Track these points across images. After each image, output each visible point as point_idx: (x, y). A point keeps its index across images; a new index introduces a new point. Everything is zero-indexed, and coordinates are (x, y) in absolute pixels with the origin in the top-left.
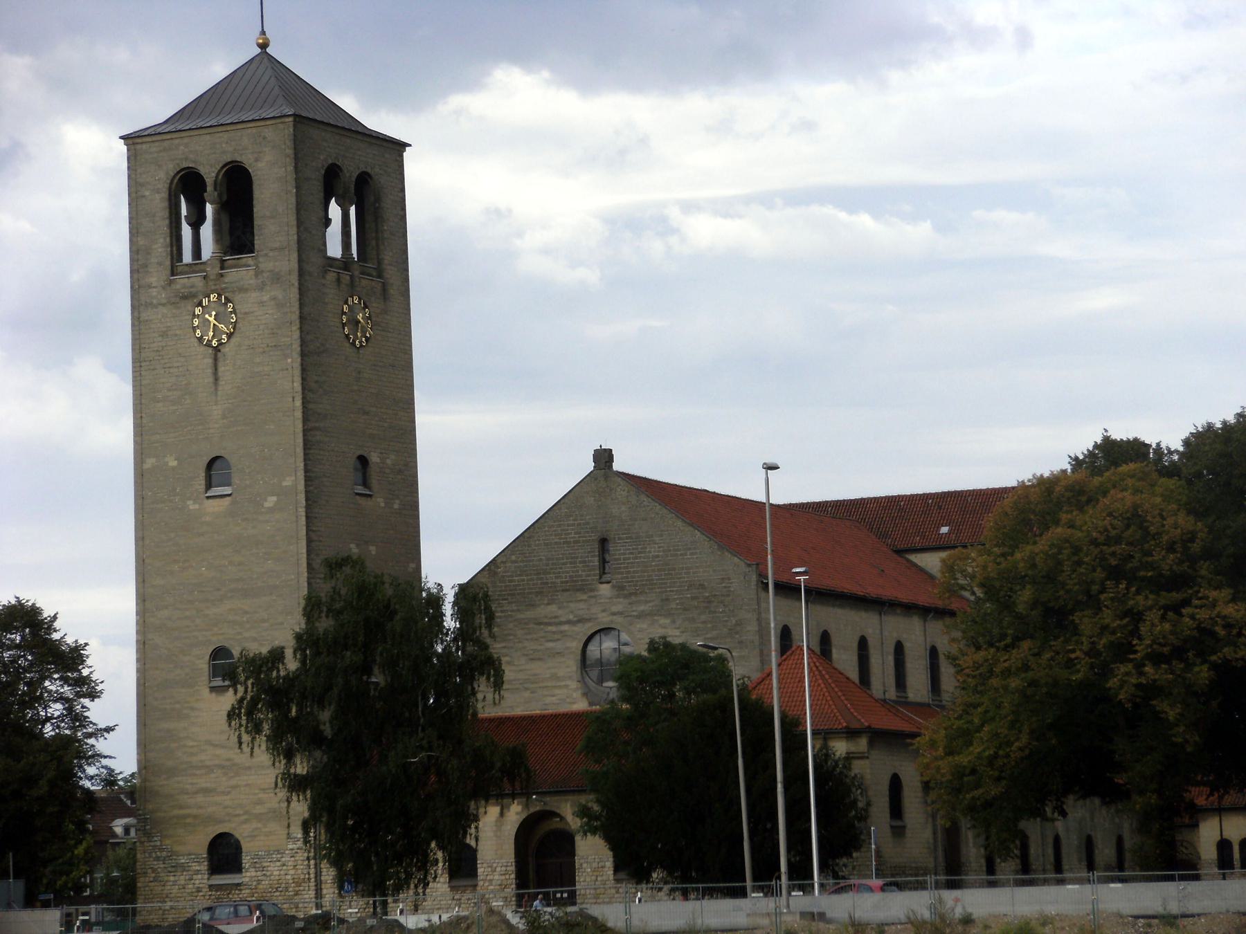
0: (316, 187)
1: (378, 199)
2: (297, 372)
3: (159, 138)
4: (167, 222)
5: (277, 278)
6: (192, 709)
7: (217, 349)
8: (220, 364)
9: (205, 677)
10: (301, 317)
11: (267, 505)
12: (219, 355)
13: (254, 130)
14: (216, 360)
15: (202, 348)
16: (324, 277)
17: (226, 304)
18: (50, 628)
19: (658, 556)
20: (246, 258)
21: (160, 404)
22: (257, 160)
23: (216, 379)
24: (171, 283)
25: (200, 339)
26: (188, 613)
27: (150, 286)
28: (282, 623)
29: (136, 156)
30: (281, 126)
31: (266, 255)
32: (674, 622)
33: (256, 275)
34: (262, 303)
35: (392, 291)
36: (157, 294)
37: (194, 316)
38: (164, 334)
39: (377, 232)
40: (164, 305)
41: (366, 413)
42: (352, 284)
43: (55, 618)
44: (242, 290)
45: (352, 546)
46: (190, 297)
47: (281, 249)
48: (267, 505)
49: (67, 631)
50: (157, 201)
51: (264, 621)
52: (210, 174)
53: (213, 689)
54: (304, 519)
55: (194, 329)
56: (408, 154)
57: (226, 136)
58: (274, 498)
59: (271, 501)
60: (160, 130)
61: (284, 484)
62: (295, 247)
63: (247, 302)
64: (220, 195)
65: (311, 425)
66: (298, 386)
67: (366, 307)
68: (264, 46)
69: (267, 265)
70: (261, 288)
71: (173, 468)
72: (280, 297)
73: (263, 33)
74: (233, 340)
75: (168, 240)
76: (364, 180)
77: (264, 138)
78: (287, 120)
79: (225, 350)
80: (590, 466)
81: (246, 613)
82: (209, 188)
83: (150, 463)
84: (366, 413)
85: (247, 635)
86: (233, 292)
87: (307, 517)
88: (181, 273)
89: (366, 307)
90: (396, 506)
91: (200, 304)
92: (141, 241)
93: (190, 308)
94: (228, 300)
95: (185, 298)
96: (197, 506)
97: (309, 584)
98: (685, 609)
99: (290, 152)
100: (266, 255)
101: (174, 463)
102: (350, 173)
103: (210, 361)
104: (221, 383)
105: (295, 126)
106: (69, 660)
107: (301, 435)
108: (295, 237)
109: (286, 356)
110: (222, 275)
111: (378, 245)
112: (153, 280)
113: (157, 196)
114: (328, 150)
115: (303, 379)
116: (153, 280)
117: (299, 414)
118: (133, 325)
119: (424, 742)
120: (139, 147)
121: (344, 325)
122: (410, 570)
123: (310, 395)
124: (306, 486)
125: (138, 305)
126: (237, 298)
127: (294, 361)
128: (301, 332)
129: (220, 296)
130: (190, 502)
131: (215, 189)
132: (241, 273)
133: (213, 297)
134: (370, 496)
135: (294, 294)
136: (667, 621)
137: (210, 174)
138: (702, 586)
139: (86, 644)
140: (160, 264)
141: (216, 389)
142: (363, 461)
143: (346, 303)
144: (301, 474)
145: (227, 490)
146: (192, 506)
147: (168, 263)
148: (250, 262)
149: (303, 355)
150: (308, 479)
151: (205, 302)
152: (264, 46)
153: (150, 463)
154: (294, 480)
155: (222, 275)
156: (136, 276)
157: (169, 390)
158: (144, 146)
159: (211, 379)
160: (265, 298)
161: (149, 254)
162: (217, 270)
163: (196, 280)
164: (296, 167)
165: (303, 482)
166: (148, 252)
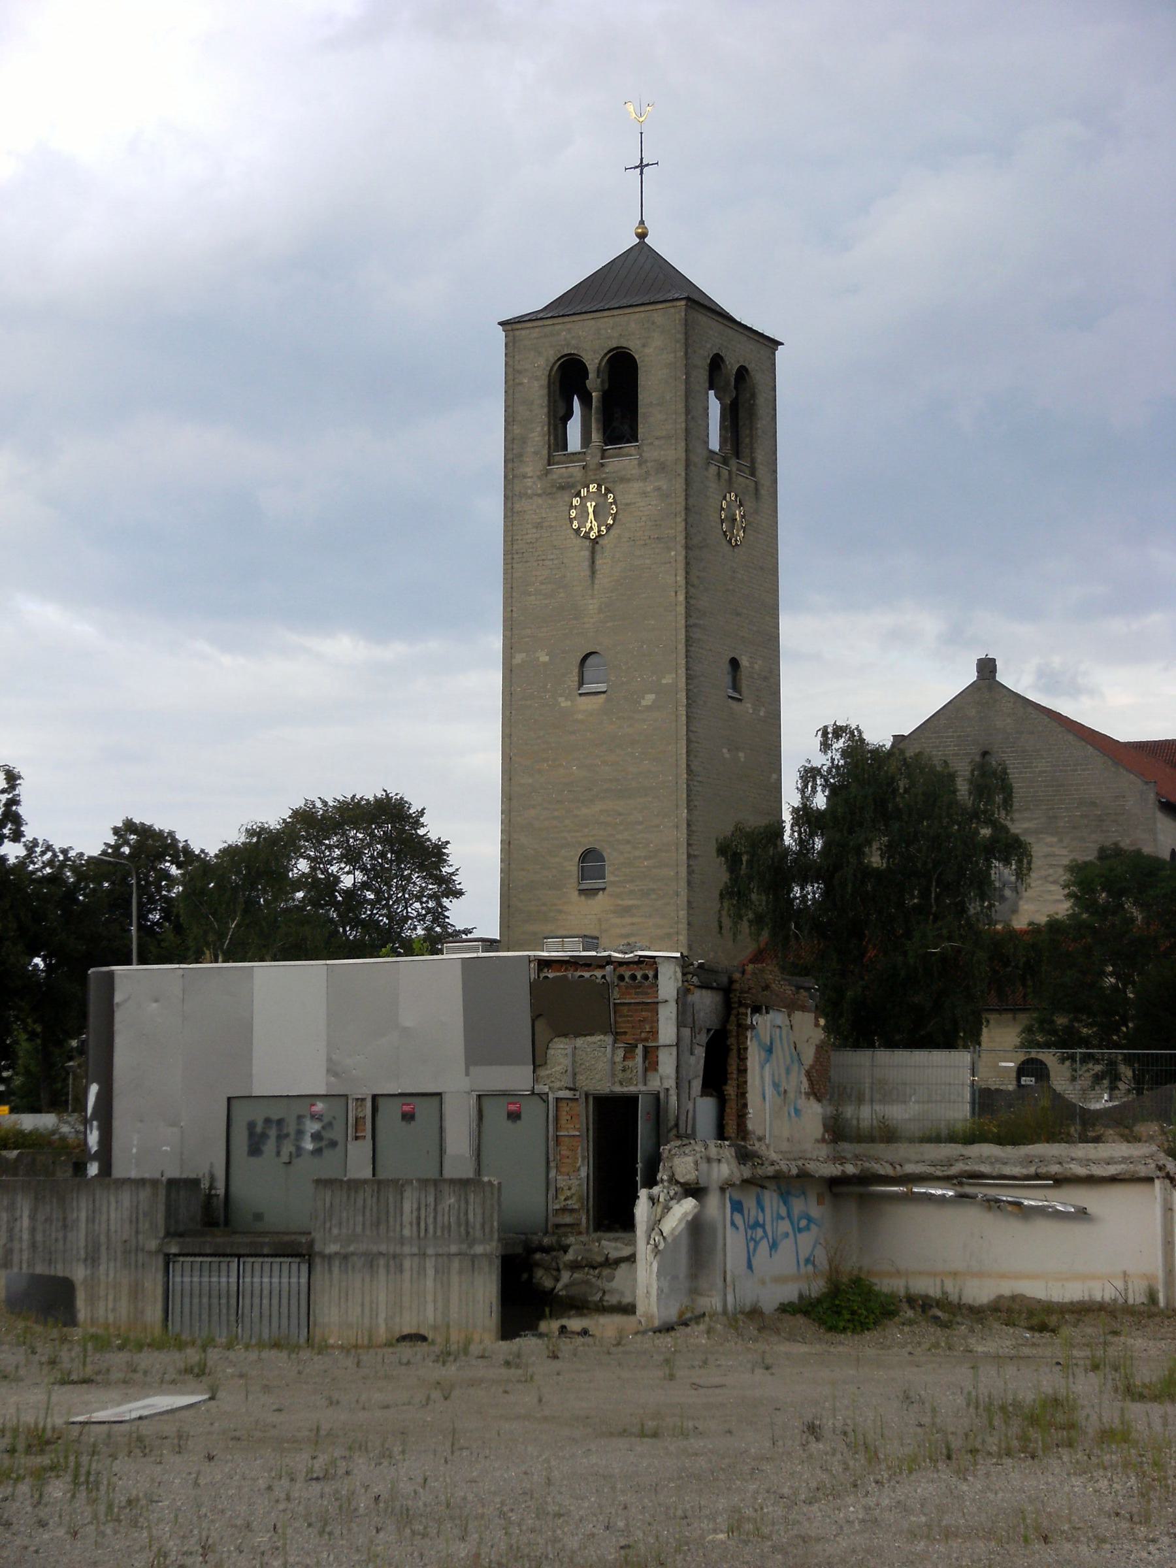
0: (701, 376)
1: (753, 396)
2: (681, 565)
3: (540, 323)
4: (546, 410)
5: (662, 467)
6: (560, 911)
7: (595, 542)
8: (598, 557)
9: (573, 881)
10: (686, 509)
11: (644, 703)
12: (598, 547)
13: (643, 315)
14: (593, 552)
15: (579, 541)
16: (707, 469)
17: (606, 494)
18: (417, 824)
19: (1045, 772)
20: (629, 447)
21: (533, 598)
22: (644, 346)
23: (593, 572)
24: (547, 473)
25: (578, 531)
26: (556, 813)
27: (525, 477)
28: (658, 826)
29: (514, 342)
30: (673, 310)
31: (651, 444)
32: (1061, 841)
33: (640, 465)
34: (645, 494)
35: (763, 492)
36: (533, 484)
37: (571, 506)
38: (538, 526)
39: (751, 429)
40: (539, 495)
41: (738, 614)
42: (730, 481)
43: (422, 813)
44: (623, 480)
45: (725, 750)
46: (570, 488)
47: (668, 437)
48: (644, 703)
49: (433, 829)
50: (537, 391)
51: (641, 823)
52: (593, 361)
53: (582, 892)
54: (684, 718)
55: (571, 520)
56: (780, 352)
57: (611, 321)
58: (653, 696)
59: (649, 699)
60: (539, 316)
61: (664, 681)
62: (682, 435)
63: (631, 492)
64: (603, 382)
65: (692, 621)
66: (681, 579)
67: (741, 505)
68: (642, 236)
69: (651, 454)
70: (644, 478)
71: (545, 664)
72: (665, 487)
73: (642, 222)
74: (612, 532)
75: (546, 429)
76: (742, 373)
77: (653, 323)
78: (678, 303)
79: (601, 541)
80: (972, 676)
81: (620, 814)
82: (592, 375)
83: (519, 658)
84: (738, 614)
85: (619, 837)
86: (614, 482)
87: (688, 717)
88: (558, 463)
89: (741, 505)
90: (762, 714)
91: (578, 494)
92: (517, 430)
93: (567, 499)
94: (608, 491)
95: (562, 488)
96: (569, 703)
97: (688, 786)
98: (1074, 828)
99: (681, 336)
100: (651, 444)
101: (547, 659)
102: (732, 365)
103: (587, 553)
104: (598, 575)
105: (686, 311)
106: (430, 857)
107: (683, 631)
108: (683, 425)
109: (669, 549)
110: (602, 465)
111: (751, 443)
112: (529, 469)
113: (536, 384)
114: (713, 339)
115: (687, 573)
116: (529, 469)
117: (681, 609)
118: (505, 517)
119: (945, 931)
120: (517, 333)
121: (722, 521)
122: (772, 781)
123: (692, 590)
124: (687, 684)
125: (510, 497)
126: (619, 488)
127: (677, 554)
128: (687, 523)
129: (599, 486)
130: (561, 699)
131: (598, 377)
132: (624, 461)
133: (593, 488)
134: (740, 700)
135: (680, 484)
136: (1055, 839)
137: (593, 361)
138: (1094, 804)
139: (448, 843)
140: (536, 453)
141: (593, 583)
142: (734, 663)
143: (725, 498)
144: (682, 671)
145: (602, 687)
146: (564, 703)
147: (545, 452)
148: (633, 451)
149: (687, 548)
150: (689, 678)
151: (584, 492)
152: (642, 236)
153: (519, 658)
154: (674, 678)
155: (602, 465)
156: (510, 466)
157: (542, 583)
158: (523, 332)
159: (588, 573)
160: (649, 489)
161: (524, 443)
162: (597, 459)
163: (575, 470)
164: (686, 353)
165: (684, 680)
166: (524, 440)
